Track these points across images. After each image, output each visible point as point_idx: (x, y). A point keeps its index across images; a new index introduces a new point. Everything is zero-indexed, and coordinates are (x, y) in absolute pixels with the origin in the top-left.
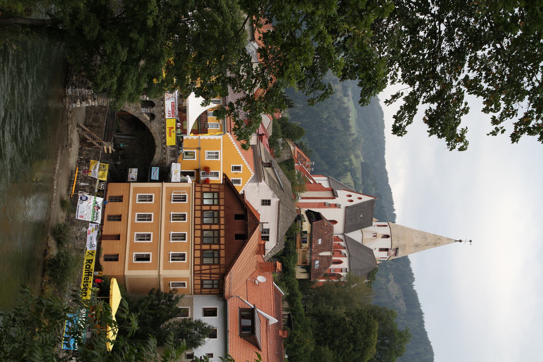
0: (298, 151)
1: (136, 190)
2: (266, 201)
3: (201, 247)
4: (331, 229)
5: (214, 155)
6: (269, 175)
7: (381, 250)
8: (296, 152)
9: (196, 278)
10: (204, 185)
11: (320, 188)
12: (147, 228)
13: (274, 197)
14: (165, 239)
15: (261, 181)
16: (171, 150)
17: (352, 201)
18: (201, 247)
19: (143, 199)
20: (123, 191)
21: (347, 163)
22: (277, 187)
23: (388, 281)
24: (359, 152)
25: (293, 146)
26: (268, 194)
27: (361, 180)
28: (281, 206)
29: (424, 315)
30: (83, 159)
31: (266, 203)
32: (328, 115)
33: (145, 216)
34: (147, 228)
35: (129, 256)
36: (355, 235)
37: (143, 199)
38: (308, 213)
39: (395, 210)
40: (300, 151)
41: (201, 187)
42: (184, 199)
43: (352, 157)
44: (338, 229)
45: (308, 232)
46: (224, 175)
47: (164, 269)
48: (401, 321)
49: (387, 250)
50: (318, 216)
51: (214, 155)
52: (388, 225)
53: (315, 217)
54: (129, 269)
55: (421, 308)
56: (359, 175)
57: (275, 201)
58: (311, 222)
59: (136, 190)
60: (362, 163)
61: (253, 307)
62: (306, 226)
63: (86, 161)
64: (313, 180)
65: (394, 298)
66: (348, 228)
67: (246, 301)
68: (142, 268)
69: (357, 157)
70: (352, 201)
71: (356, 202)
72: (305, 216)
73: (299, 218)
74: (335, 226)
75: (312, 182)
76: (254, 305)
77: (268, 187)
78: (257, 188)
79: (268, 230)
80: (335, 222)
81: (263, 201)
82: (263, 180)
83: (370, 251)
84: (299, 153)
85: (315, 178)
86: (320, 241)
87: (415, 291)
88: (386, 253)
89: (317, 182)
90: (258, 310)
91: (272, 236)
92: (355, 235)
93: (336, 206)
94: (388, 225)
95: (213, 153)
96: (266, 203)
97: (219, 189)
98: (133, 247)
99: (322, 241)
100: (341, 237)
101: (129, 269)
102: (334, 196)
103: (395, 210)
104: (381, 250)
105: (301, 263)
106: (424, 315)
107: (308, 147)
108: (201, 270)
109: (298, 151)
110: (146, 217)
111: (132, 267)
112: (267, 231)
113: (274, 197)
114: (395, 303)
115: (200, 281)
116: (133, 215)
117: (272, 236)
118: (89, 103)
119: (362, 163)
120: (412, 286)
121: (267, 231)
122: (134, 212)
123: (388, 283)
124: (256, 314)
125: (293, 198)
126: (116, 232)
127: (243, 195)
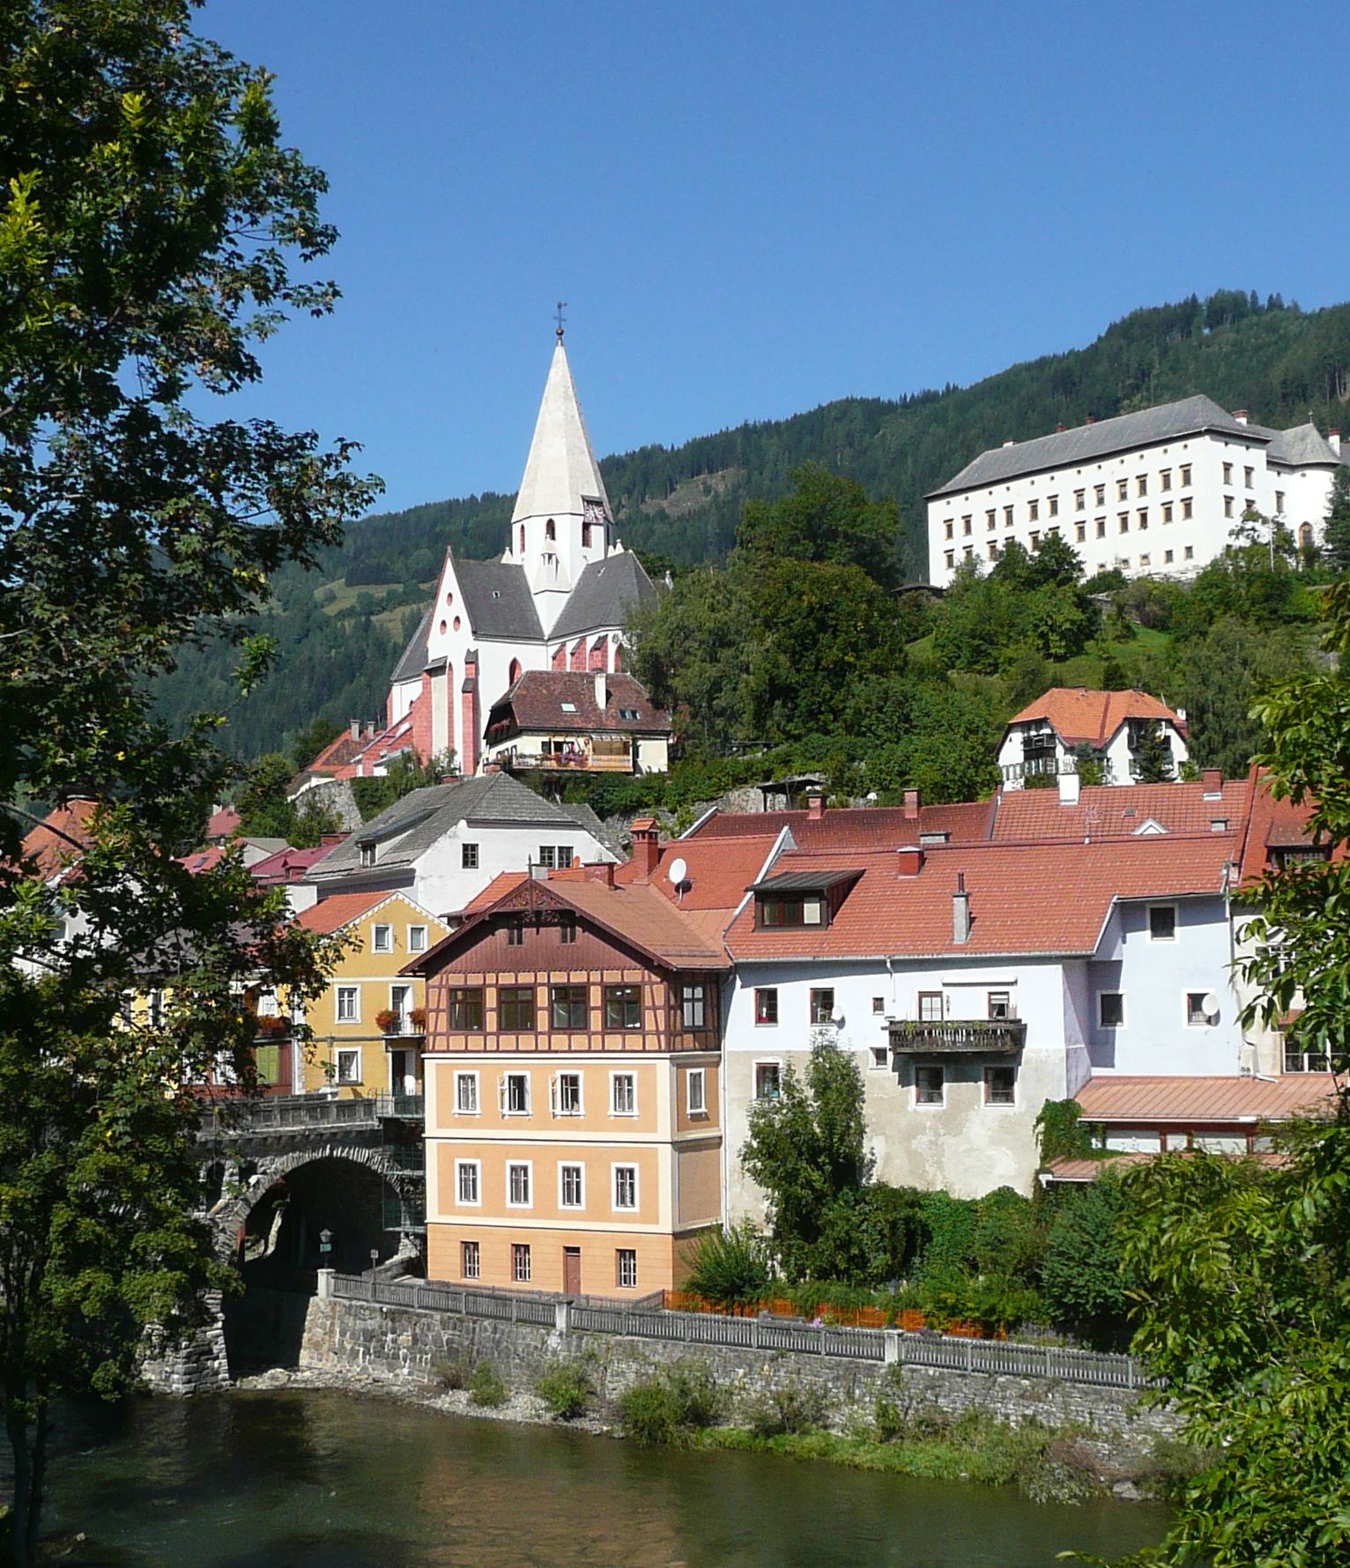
0: (324, 764)
1: (446, 1207)
2: (465, 856)
3: (595, 1033)
4: (533, 676)
5: (346, 999)
6: (396, 849)
7: (586, 542)
8: (325, 769)
9: (678, 1047)
10: (431, 1029)
11: (420, 707)
12: (599, 1182)
13: (455, 836)
14: (577, 1128)
15: (413, 871)
16: (338, 1115)
17: (457, 619)
18: (595, 1033)
19: (469, 1191)
20: (450, 1241)
21: (349, 624)
22: (425, 826)
23: (662, 515)
24: (319, 594)
25: (308, 779)
26: (448, 847)
27: (393, 586)
28: (480, 815)
29: (751, 422)
30: (365, 1346)
31: (470, 856)
32: (217, 678)
33: (515, 1183)
34: (599, 1182)
35: (623, 1224)
36: (549, 612)
37: (469, 1191)
38: (494, 738)
39: (473, 497)
40: (324, 757)
41: (436, 1034)
42: (518, 1082)
43: (331, 610)
44: (536, 658)
45: (546, 739)
46: (402, 974)
47: (655, 1130)
48: (767, 482)
49: (586, 526)
50: (502, 711)
51: (346, 999)
52: (519, 525)
53: (504, 722)
54: (656, 1221)
55: (732, 428)
56: (380, 592)
57: (463, 833)
58: (518, 733)
59: (446, 1207)
60: (349, 584)
61: (750, 894)
62: (529, 746)
63: (370, 1341)
64: (401, 722)
65: (708, 499)
66: (527, 631)
67: (737, 911)
68: (652, 1186)
69: (331, 598)
70: (457, 619)
71: (459, 607)
72: (501, 747)
73: (505, 764)
74: (525, 667)
75: (405, 726)
76: (747, 890)
77: (429, 851)
78: (430, 880)
79: (543, 849)
80: (514, 665)
81: (465, 864)
82: (412, 866)
83: (592, 569)
84: (328, 759)
85: (395, 721)
86: (568, 707)
87: (688, 445)
88: (593, 528)
89: (406, 711)
90: (758, 881)
91: (557, 838)
92: (549, 612)
93: (472, 659)
94: (519, 525)
95: (341, 1002)
96: (470, 856)
97: (440, 987)
98: (598, 1212)
99: (567, 702)
100: (553, 649)
101: (656, 1221)
102: (440, 669)
103: (473, 497)
104: (586, 542)
105: (626, 757)
106: (751, 422)
107: (308, 731)
108: (658, 1033)
109: (324, 764)
110: (517, 1182)
111: (651, 1215)
112: (546, 852)
113: (455, 836)
114: (721, 498)
115: (685, 1036)
116: (513, 1214)
117: (557, 838)
118: (218, 1336)
119: (349, 584)
120: (675, 454)
121: (546, 852)
122: (502, 1212)
123: (667, 517)
124: (769, 885)
125: (457, 784)
126: (457, 1250)
127: (453, 919)
